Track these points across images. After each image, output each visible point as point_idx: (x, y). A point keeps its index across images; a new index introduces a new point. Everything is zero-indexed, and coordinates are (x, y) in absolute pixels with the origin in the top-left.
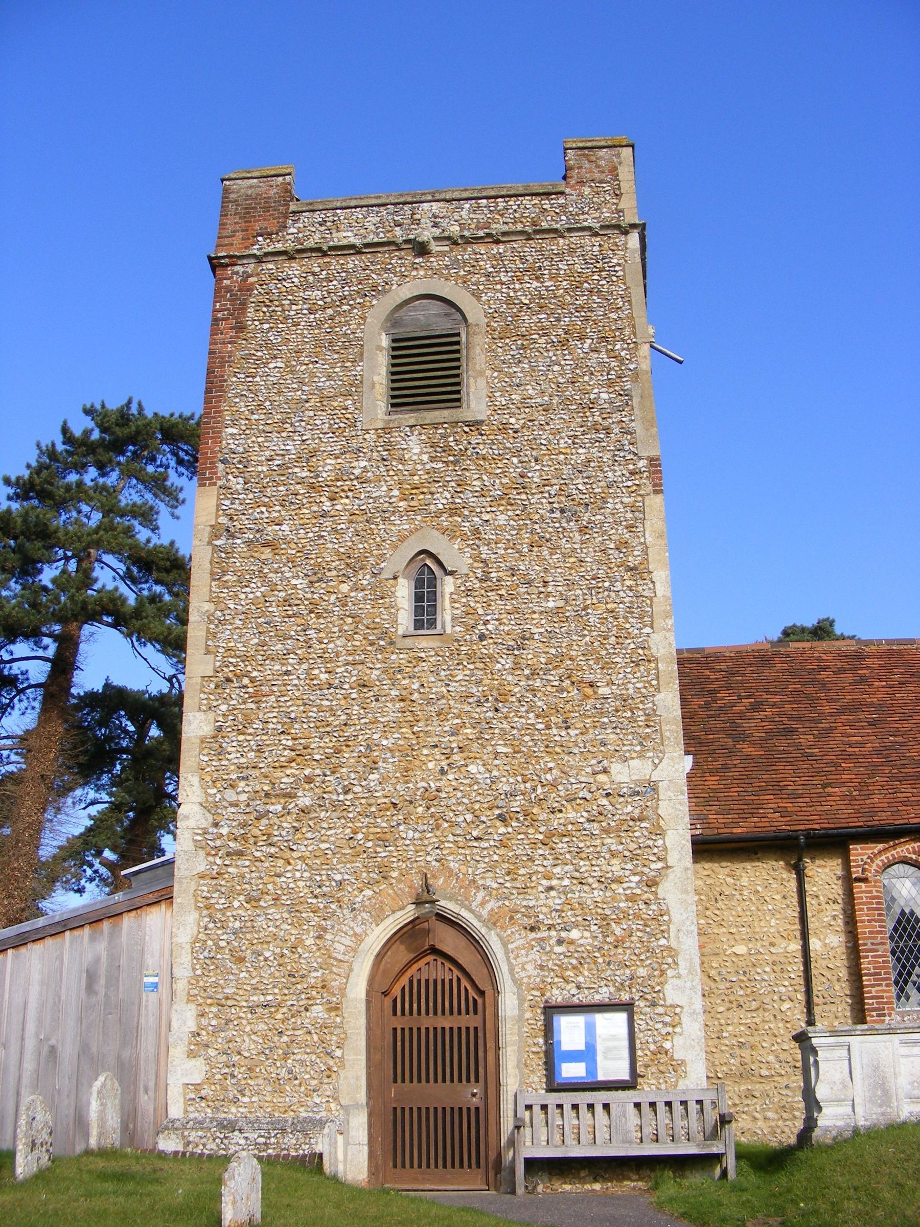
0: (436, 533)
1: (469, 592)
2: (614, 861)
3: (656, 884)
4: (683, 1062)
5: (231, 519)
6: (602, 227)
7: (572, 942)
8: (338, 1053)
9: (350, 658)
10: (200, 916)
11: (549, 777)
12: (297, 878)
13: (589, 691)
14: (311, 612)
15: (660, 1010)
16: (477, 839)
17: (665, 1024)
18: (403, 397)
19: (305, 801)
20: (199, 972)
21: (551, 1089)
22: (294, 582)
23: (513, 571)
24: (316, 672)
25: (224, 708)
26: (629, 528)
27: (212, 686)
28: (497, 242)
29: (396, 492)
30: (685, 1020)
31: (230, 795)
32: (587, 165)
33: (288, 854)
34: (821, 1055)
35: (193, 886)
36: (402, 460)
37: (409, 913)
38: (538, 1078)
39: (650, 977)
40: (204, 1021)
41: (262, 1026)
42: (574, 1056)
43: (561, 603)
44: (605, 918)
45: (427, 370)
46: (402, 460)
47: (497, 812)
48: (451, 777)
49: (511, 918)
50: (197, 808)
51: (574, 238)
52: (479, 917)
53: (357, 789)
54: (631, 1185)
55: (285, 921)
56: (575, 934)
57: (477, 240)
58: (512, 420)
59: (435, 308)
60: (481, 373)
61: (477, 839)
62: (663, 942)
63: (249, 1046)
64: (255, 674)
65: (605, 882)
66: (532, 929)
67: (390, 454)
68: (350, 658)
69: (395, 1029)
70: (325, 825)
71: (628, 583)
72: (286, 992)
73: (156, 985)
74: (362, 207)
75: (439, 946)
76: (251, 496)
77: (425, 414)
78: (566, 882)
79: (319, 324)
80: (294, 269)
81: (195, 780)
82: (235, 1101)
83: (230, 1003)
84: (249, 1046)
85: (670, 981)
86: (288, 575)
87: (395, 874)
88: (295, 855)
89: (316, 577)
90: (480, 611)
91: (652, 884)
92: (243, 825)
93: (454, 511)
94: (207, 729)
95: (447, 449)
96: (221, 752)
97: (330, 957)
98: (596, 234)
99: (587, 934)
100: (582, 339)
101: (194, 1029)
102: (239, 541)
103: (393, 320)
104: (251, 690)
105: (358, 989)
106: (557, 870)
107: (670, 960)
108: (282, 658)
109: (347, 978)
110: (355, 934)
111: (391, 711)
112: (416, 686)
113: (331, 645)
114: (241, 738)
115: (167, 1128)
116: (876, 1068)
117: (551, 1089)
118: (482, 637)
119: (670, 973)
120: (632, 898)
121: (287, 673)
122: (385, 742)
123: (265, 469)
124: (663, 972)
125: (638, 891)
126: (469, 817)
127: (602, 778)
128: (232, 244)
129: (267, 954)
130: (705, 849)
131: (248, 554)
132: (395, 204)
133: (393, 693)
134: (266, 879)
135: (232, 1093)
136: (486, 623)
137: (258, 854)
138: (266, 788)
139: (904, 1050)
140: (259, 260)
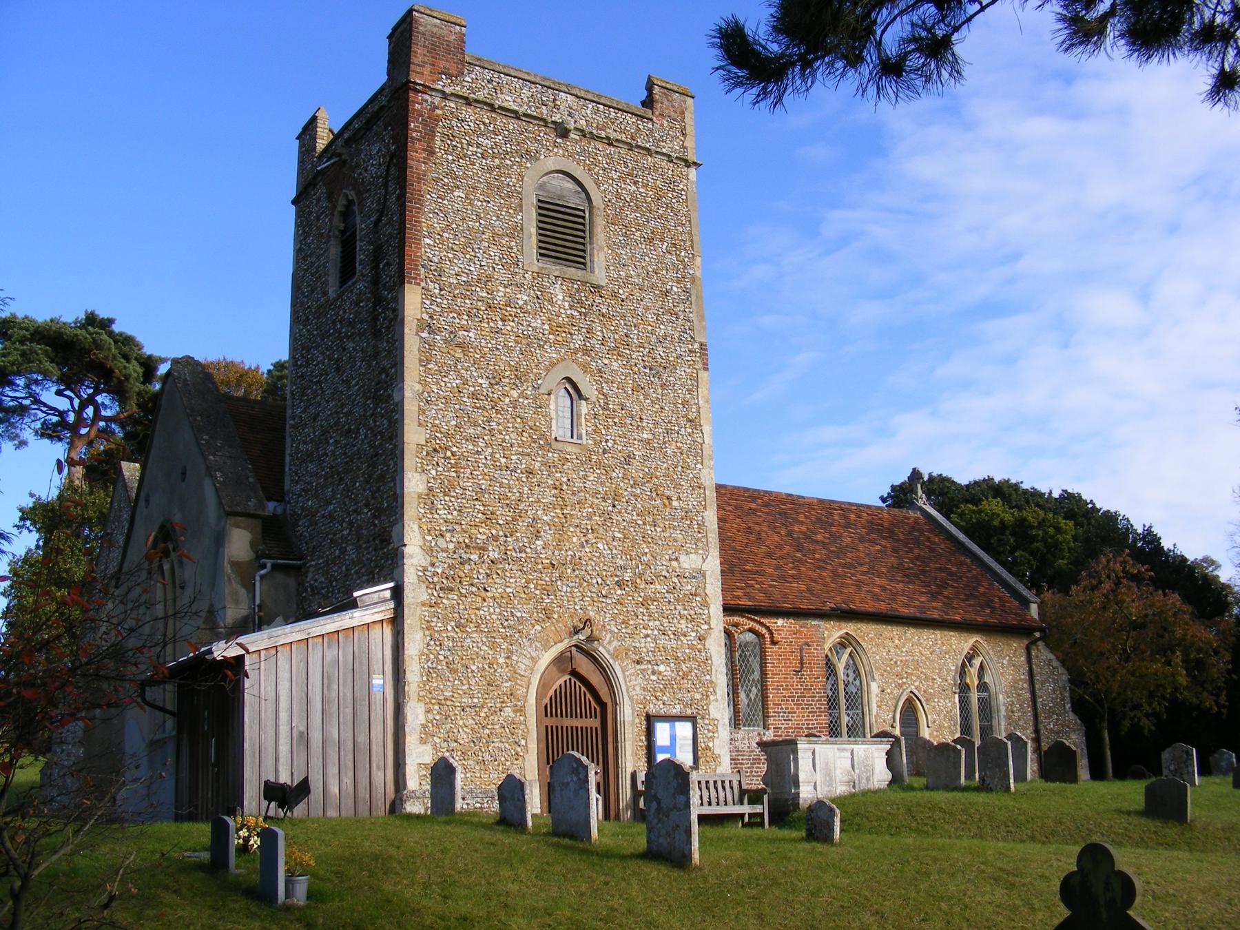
7: (660, 673)
8: (523, 742)
12: (490, 611)
15: (707, 722)
18: (547, 250)
19: (494, 555)
22: (480, 381)
28: (610, 144)
29: (547, 327)
30: (720, 728)
33: (483, 593)
34: (800, 754)
35: (418, 612)
40: (430, 716)
42: (664, 749)
43: (651, 437)
44: (677, 658)
45: (564, 233)
46: (551, 302)
50: (418, 550)
52: (608, 651)
53: (528, 550)
56: (662, 668)
59: (570, 185)
60: (601, 249)
64: (454, 449)
67: (542, 297)
80: (468, 113)
81: (416, 527)
83: (449, 703)
88: (489, 594)
89: (496, 380)
92: (451, 567)
93: (586, 352)
94: (422, 488)
95: (581, 302)
96: (432, 508)
98: (671, 161)
106: (651, 624)
108: (473, 439)
110: (532, 658)
111: (549, 496)
114: (447, 498)
116: (827, 764)
119: (712, 698)
120: (691, 647)
126: (600, 581)
127: (675, 564)
129: (474, 668)
130: (728, 610)
132: (543, 86)
136: (607, 441)
137: (464, 591)
139: (838, 754)
140: (445, 96)
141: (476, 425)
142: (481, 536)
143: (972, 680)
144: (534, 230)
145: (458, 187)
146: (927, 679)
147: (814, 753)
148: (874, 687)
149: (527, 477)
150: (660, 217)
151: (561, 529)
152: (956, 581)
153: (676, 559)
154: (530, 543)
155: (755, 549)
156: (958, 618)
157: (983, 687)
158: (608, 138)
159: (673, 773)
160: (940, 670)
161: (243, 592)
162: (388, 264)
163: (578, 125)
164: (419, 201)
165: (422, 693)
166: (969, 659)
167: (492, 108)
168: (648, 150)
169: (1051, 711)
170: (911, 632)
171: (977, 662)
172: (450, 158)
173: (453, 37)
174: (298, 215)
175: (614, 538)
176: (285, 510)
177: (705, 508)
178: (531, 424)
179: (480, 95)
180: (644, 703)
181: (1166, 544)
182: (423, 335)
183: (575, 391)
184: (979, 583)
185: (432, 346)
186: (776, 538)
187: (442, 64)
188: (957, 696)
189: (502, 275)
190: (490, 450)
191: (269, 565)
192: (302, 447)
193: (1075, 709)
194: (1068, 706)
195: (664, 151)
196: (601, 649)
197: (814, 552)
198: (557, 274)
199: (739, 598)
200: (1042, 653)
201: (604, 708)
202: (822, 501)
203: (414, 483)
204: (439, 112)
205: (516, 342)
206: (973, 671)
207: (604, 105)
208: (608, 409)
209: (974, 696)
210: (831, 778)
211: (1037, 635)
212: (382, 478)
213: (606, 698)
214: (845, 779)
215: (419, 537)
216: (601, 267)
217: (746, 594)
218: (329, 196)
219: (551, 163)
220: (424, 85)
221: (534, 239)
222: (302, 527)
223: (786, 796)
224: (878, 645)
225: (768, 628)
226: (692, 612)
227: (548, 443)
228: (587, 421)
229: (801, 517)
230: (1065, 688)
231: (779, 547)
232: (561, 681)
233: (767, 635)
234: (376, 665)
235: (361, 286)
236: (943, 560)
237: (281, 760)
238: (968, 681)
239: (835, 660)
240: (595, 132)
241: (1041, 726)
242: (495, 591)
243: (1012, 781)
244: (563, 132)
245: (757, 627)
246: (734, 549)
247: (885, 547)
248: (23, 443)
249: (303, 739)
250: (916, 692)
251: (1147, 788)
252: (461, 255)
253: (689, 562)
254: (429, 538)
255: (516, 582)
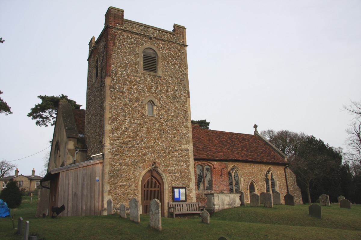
0: (153, 97)
1: (158, 110)
2: (182, 162)
3: (188, 167)
4: (193, 198)
5: (114, 85)
6: (181, 44)
7: (176, 176)
8: (137, 195)
9: (138, 118)
10: (110, 167)
11: (172, 146)
12: (129, 160)
13: (178, 131)
14: (130, 108)
16: (161, 156)
17: (190, 191)
18: (146, 68)
19: (130, 145)
20: (110, 178)
21: (173, 201)
22: (127, 101)
23: (166, 107)
24: (131, 120)
25: (113, 124)
26: (185, 103)
27: (111, 119)
28: (163, 41)
29: (145, 87)
30: (193, 190)
31: (115, 143)
32: (178, 30)
33: (127, 156)
34: (215, 197)
35: (108, 160)
36: (146, 81)
37: (150, 168)
38: (171, 200)
39: (188, 183)
41: (123, 189)
43: (174, 115)
44: (181, 172)
46: (146, 81)
47: (164, 151)
48: (156, 144)
49: (167, 171)
50: (109, 145)
51: (176, 45)
52: (161, 170)
53: (139, 144)
54: (186, 219)
55: (127, 169)
56: (176, 175)
57: (160, 39)
58: (166, 78)
59: (152, 51)
60: (160, 67)
61: (161, 156)
62: (190, 177)
63: (120, 193)
64: (119, 118)
65: (181, 166)
66: (170, 173)
68: (138, 118)
69: (145, 190)
70: (134, 150)
71: (184, 113)
72: (127, 182)
73: (98, 180)
74: (138, 25)
75: (153, 175)
76: (117, 81)
77: (150, 73)
78: (175, 165)
79: (130, 48)
81: (108, 139)
82: (118, 204)
83: (116, 184)
84: (120, 193)
85: (191, 184)
86: (125, 99)
87: (147, 161)
88: (128, 156)
89: (131, 101)
90: (161, 114)
91: (188, 167)
92: (118, 149)
93: (156, 93)
94: (110, 129)
95: (154, 81)
96: (113, 134)
97: (135, 176)
98: (180, 45)
99: (178, 175)
100: (177, 65)
101: (109, 189)
102: (115, 90)
103: (144, 52)
104: (119, 122)
105: (140, 183)
106: (173, 163)
107: (190, 180)
109: (139, 180)
110: (140, 172)
112: (150, 126)
113: (134, 115)
114: (117, 131)
115: (105, 210)
116: (222, 200)
117: (173, 201)
118: (161, 119)
120: (185, 169)
121: (126, 119)
122: (144, 136)
123: (120, 76)
124: (190, 182)
125: (186, 168)
126: (159, 152)
127: (180, 147)
128: (112, 24)
129: (124, 175)
130: (195, 159)
131: (117, 93)
133: (146, 127)
134: (123, 160)
135: (117, 202)
136: (162, 116)
137: (121, 155)
138: (122, 142)
139: (226, 197)
140: (118, 30)
141: (125, 112)
142: (126, 140)
143: (269, 177)
144: (142, 63)
145: (121, 52)
146: (256, 177)
147: (219, 197)
148: (242, 179)
149: (139, 125)
150: (177, 59)
151: (148, 138)
152: (265, 152)
153: (181, 146)
154: (140, 142)
155: (210, 145)
156: (265, 161)
157: (272, 179)
158: (162, 39)
159: (155, 203)
160: (260, 175)
161: (71, 157)
162: (104, 72)
163: (154, 36)
164: (110, 56)
165: (109, 182)
166: (268, 172)
167: (131, 32)
168: (173, 42)
169: (291, 186)
170: (252, 165)
171: (270, 173)
172: (119, 45)
173: (120, 15)
174: (89, 63)
175: (163, 141)
176: (84, 136)
177: (189, 133)
178: (141, 112)
179: (128, 29)
180: (172, 184)
181: (325, 143)
182: (111, 89)
183: (152, 103)
184: (271, 152)
185: (114, 92)
186: (217, 142)
187: (117, 21)
188: (265, 182)
189: (134, 74)
190: (129, 119)
191: (78, 150)
192: (88, 120)
193: (298, 185)
194: (296, 184)
195: (178, 42)
196: (159, 169)
197: (227, 145)
198: (148, 74)
199: (204, 157)
200: (288, 170)
201: (160, 185)
202: (230, 133)
203: (108, 127)
204: (116, 33)
205: (137, 91)
206: (269, 175)
207: (161, 31)
208: (162, 108)
209: (270, 182)
210: (224, 203)
211: (287, 165)
212: (101, 126)
213: (161, 183)
214: (228, 204)
215: (109, 141)
216: (160, 71)
217: (207, 156)
218: (94, 58)
219: (147, 46)
220: (112, 27)
221: (142, 65)
222: (87, 141)
223: (211, 208)
224: (243, 168)
225: (212, 164)
226: (185, 160)
227: (145, 117)
228: (156, 111)
229: (224, 137)
230: (295, 179)
231: (217, 144)
232: (149, 178)
233: (212, 166)
234: (97, 175)
235: (99, 79)
236: (262, 147)
237: (69, 200)
238: (268, 177)
239: (231, 172)
240: (159, 38)
241: (289, 189)
242: (130, 155)
243: (272, 204)
244: (151, 39)
245: (210, 164)
246: (205, 145)
247: (246, 144)
248: (47, 126)
249: (75, 195)
250: (254, 180)
251: (310, 207)
252: (122, 69)
253: (184, 147)
254: (112, 141)
255: (135, 152)
